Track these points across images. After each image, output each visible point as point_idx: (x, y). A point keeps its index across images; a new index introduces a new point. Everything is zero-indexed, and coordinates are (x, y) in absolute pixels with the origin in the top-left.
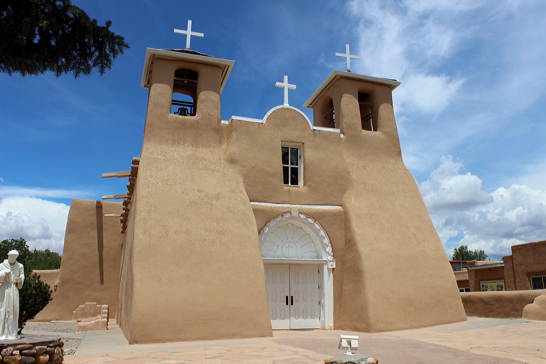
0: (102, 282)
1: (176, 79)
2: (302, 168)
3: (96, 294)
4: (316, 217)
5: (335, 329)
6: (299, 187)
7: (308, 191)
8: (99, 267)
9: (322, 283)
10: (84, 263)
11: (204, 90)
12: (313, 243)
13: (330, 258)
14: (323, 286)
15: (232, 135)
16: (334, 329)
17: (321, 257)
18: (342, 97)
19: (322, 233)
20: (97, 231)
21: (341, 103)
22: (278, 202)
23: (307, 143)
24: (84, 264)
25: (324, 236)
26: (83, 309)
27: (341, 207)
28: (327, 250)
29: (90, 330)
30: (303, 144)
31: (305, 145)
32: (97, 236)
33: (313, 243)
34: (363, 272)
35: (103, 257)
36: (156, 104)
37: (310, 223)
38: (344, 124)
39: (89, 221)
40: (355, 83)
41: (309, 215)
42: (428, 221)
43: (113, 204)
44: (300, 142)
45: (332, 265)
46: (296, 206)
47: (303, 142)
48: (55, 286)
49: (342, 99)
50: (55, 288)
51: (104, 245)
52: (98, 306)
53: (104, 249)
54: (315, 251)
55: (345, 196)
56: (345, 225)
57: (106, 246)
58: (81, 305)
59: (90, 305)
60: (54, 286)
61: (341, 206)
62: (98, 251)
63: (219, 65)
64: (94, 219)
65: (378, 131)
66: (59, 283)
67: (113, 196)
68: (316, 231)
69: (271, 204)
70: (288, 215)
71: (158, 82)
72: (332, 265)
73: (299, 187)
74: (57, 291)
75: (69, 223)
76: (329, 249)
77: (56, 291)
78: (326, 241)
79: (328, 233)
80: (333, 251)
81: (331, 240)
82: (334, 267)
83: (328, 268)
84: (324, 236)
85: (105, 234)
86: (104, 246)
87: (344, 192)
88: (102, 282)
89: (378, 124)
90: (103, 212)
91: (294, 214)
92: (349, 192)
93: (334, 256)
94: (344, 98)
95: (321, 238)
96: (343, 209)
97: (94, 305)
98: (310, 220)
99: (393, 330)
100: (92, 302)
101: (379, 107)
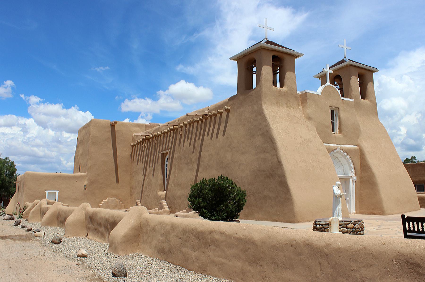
0: (118, 181)
1: (273, 63)
2: (337, 122)
3: (114, 192)
4: (347, 151)
5: (357, 214)
6: (335, 133)
7: (343, 137)
8: (115, 171)
9: (348, 189)
10: (104, 168)
11: (289, 71)
12: (342, 166)
13: (354, 175)
14: (349, 190)
15: (307, 102)
16: (356, 214)
17: (347, 174)
18: (351, 78)
19: (350, 161)
20: (112, 144)
21: (351, 82)
22: (331, 143)
23: (341, 108)
24: (105, 169)
25: (351, 163)
26: (107, 203)
27: (357, 146)
28: (352, 171)
29: (191, 217)
30: (339, 108)
31: (340, 109)
32: (112, 148)
33: (342, 166)
34: (377, 184)
35: (118, 164)
36: (266, 80)
37: (345, 155)
38: (353, 95)
39: (106, 136)
40: (357, 69)
41: (345, 151)
42: (397, 156)
43: (122, 124)
44: (337, 107)
45: (355, 179)
46: (339, 145)
47: (338, 107)
48: (85, 186)
49: (351, 79)
50: (85, 187)
51: (118, 155)
52: (117, 200)
53: (118, 158)
54: (343, 171)
55: (359, 140)
56: (361, 157)
57: (119, 155)
58: (104, 200)
59: (112, 200)
60: (84, 186)
61: (357, 146)
62: (114, 159)
63: (293, 55)
64: (109, 135)
65: (366, 99)
66: (88, 183)
67: (166, 123)
68: (347, 160)
69: (328, 144)
70: (336, 151)
71: (266, 65)
72: (355, 179)
73: (335, 133)
74: (86, 189)
75: (92, 137)
76: (353, 170)
77: (86, 190)
78: (352, 166)
79: (353, 161)
80: (355, 171)
81: (354, 165)
82: (356, 180)
83: (352, 181)
84: (351, 163)
85: (118, 147)
86: (118, 156)
87: (358, 137)
88: (118, 181)
89: (366, 95)
90: (116, 129)
91: (339, 150)
92: (360, 137)
93: (355, 174)
94: (353, 79)
95: (349, 164)
96: (358, 148)
97: (114, 200)
98: (345, 154)
99: (394, 214)
100: (112, 197)
101: (368, 84)
